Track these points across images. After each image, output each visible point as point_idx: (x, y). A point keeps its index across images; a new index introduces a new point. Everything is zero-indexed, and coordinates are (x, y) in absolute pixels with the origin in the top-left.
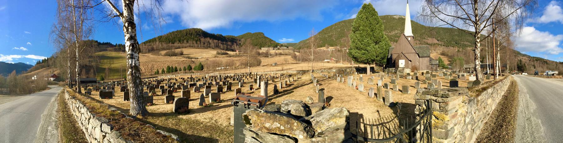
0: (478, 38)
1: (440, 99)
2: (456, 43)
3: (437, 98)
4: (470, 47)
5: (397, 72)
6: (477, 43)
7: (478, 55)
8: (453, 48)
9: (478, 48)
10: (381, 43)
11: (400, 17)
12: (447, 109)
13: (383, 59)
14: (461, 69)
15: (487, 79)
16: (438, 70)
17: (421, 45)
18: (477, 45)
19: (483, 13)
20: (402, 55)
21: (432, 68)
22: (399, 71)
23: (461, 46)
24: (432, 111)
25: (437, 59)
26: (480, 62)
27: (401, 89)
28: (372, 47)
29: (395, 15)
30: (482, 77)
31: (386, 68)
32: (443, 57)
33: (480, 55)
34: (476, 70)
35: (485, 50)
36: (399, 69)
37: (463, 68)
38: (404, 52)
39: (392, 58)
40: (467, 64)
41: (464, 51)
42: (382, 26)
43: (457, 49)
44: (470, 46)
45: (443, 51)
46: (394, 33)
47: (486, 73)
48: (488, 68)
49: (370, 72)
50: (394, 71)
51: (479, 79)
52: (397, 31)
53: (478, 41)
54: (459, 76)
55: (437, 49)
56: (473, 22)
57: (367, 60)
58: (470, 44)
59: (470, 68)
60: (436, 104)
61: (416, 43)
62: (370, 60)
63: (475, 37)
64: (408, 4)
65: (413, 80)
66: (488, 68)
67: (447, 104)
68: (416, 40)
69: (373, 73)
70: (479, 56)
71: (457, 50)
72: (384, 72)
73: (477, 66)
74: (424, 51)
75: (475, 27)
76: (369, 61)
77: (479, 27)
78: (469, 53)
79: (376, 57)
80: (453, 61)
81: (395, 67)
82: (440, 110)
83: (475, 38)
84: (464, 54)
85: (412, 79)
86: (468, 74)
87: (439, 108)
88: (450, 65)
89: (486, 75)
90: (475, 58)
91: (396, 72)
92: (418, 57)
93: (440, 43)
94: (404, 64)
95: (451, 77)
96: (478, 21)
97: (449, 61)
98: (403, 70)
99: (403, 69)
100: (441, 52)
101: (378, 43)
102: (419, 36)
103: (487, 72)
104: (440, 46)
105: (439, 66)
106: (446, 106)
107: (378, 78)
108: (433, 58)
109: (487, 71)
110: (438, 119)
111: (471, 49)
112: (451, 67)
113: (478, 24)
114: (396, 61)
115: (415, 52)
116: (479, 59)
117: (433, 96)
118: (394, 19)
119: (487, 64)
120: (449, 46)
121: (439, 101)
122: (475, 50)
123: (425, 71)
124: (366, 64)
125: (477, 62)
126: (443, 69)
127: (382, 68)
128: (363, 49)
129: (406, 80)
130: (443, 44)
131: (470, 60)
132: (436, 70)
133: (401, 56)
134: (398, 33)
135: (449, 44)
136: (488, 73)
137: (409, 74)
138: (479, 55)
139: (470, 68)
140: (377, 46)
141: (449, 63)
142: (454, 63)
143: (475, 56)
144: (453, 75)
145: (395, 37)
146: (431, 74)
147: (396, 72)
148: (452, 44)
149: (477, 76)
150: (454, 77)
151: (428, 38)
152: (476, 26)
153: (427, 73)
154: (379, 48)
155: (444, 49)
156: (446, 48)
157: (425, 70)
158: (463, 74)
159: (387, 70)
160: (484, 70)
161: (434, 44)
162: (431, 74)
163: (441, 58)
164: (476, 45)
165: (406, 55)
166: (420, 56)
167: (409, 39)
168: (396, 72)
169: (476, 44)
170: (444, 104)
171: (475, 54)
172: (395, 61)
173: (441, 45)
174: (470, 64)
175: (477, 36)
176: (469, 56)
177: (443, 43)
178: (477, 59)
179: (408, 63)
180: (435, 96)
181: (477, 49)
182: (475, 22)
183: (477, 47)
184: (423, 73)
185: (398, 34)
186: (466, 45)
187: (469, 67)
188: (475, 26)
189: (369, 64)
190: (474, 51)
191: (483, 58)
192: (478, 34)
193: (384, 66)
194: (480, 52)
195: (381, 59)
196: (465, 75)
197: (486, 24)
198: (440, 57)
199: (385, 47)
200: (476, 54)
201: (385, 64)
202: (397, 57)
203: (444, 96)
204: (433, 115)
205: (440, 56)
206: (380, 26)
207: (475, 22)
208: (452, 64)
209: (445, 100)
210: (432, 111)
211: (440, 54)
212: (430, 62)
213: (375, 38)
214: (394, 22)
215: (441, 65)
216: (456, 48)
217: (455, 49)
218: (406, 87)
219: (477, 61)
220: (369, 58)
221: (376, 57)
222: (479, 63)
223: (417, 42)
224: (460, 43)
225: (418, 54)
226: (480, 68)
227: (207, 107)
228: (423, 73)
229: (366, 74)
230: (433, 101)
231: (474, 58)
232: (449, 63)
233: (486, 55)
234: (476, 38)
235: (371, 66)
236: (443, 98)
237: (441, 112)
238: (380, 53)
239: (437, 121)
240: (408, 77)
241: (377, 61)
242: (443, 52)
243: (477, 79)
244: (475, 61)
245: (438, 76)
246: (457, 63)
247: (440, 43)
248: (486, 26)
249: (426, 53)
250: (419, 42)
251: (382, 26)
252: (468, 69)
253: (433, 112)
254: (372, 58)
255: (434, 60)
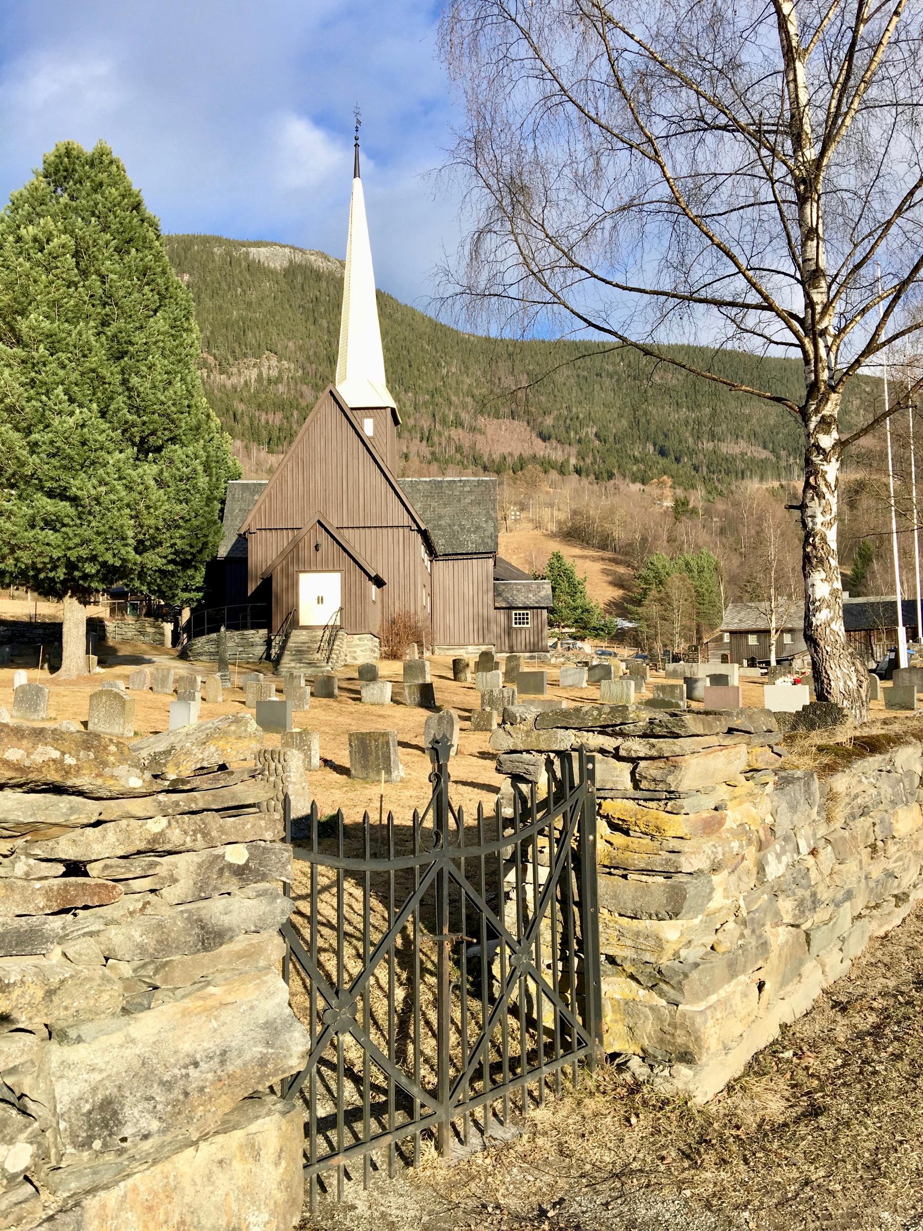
0: (825, 424)
1: (637, 747)
2: (663, 452)
3: (620, 740)
4: (762, 479)
5: (286, 660)
6: (817, 459)
7: (824, 539)
8: (638, 486)
9: (824, 489)
10: (176, 451)
11: (298, 258)
12: (677, 786)
13: (186, 564)
14: (700, 639)
15: (890, 705)
16: (550, 642)
17: (435, 467)
18: (815, 473)
19: (866, 245)
20: (323, 538)
21: (509, 631)
22: (300, 653)
23: (696, 469)
24: (598, 801)
25: (546, 571)
26: (838, 585)
27: (343, 758)
28: (112, 478)
29: (258, 244)
30: (853, 685)
31: (197, 628)
32: (577, 551)
33: (840, 535)
34: (816, 635)
35: (880, 495)
36: (297, 638)
37: (717, 632)
38: (333, 522)
39: (244, 561)
40: (738, 600)
41: (720, 506)
42: (189, 330)
43: (668, 492)
44: (760, 469)
45: (575, 513)
46: (254, 373)
47: (890, 670)
48: (902, 631)
49: (87, 653)
50: (260, 650)
51: (836, 697)
52: (274, 361)
53: (826, 441)
54: (690, 682)
55: (543, 498)
56: (788, 317)
57: (71, 566)
58: (765, 454)
59: (768, 632)
60: (615, 769)
61: (406, 457)
62: (90, 569)
63: (806, 419)
64: (357, 182)
65: (400, 708)
66: (902, 631)
67: (671, 762)
68: (406, 434)
69: (101, 663)
70: (834, 546)
71: (668, 503)
72: (183, 656)
73: (818, 609)
74: (464, 511)
75: (805, 352)
76: (86, 577)
77: (828, 349)
78: (761, 519)
79: (140, 548)
80: (646, 580)
81: (268, 625)
82: (638, 794)
83: (807, 426)
84: (722, 531)
85: (395, 701)
86: (756, 672)
87: (629, 785)
88: (624, 614)
89: (889, 684)
90: (807, 558)
91: (272, 662)
92: (426, 557)
93: (556, 454)
94: (334, 601)
95: (638, 688)
96: (824, 313)
97: (619, 583)
98: (331, 642)
99: (333, 632)
100: (561, 516)
101: (159, 449)
102: (425, 403)
103: (894, 663)
104: (554, 475)
105: (555, 617)
106: (671, 772)
107: (151, 696)
108: (515, 561)
109: (896, 651)
110: (626, 832)
111: (773, 492)
112: (627, 624)
113: (823, 333)
114: (278, 584)
115: (407, 521)
116: (834, 562)
117: (600, 733)
118: (255, 269)
119: (894, 603)
120: (611, 476)
121: (629, 750)
122: (803, 507)
123: (470, 654)
124: (60, 597)
125: (818, 583)
126: (582, 639)
127: (168, 627)
128: (41, 488)
129: (359, 706)
130: (573, 461)
131: (767, 570)
132: (536, 648)
133: (317, 548)
134: (278, 380)
135: (612, 461)
136: (904, 663)
137: (368, 674)
138: (832, 536)
139: (768, 632)
140: (149, 470)
141: (618, 593)
142: (653, 593)
143: (806, 543)
144: (650, 680)
145: (259, 406)
146: (511, 675)
147: (280, 656)
148: (636, 461)
149: (818, 675)
150: (662, 688)
151: (482, 421)
152: (809, 347)
153: (486, 662)
154: (161, 483)
155: (577, 493)
156: (596, 487)
157: (471, 649)
158: (722, 669)
159: (201, 643)
160: (869, 645)
161: (521, 464)
162: (506, 674)
163: (568, 562)
164: (810, 469)
165: (350, 538)
166: (440, 545)
167: (368, 427)
168: (277, 662)
169: (808, 462)
170: (662, 765)
171: (802, 533)
172: (267, 582)
173: (562, 470)
174: (764, 605)
175: (817, 411)
176: (760, 539)
177: (574, 450)
178: (821, 561)
179: (364, 596)
180: (614, 735)
181: (821, 496)
182: (801, 322)
183: (815, 488)
184: (458, 667)
185: (281, 388)
186: (729, 460)
187: (761, 625)
188: (802, 346)
189: (84, 596)
190: (797, 513)
191: (865, 558)
192: (825, 399)
193: (186, 614)
194: (839, 517)
195: (172, 562)
196: (734, 681)
197: (879, 328)
198: (558, 557)
199: (203, 481)
200: (809, 534)
201: (188, 601)
202: (284, 555)
203: (657, 730)
204: (602, 817)
205: (555, 546)
206: (177, 328)
207: (801, 322)
208: (639, 603)
209: (663, 745)
210: (598, 801)
211: (553, 536)
212: (497, 593)
213: (138, 411)
214: (253, 296)
215: (566, 612)
216: (661, 484)
217: (656, 492)
218: (385, 739)
219: (817, 577)
220: (84, 552)
221: (136, 550)
222: (834, 593)
223: (413, 450)
224: (692, 453)
225: (424, 534)
226: (839, 627)
227: (292, 247)
228: (458, 667)
229: (54, 668)
230: (598, 756)
231: (794, 560)
232: (618, 593)
233: (883, 538)
234: (812, 426)
235: (93, 611)
236: (652, 740)
237: (641, 802)
238: (172, 525)
239: (619, 839)
240: (369, 692)
241: (142, 576)
242: (581, 522)
243: (821, 694)
244: (806, 576)
245: (555, 684)
246: (675, 594)
247: (556, 454)
248: (883, 338)
249: (478, 528)
250: (425, 450)
251: (189, 330)
252: (752, 640)
253: (600, 805)
254: (109, 558)
255: (522, 576)
